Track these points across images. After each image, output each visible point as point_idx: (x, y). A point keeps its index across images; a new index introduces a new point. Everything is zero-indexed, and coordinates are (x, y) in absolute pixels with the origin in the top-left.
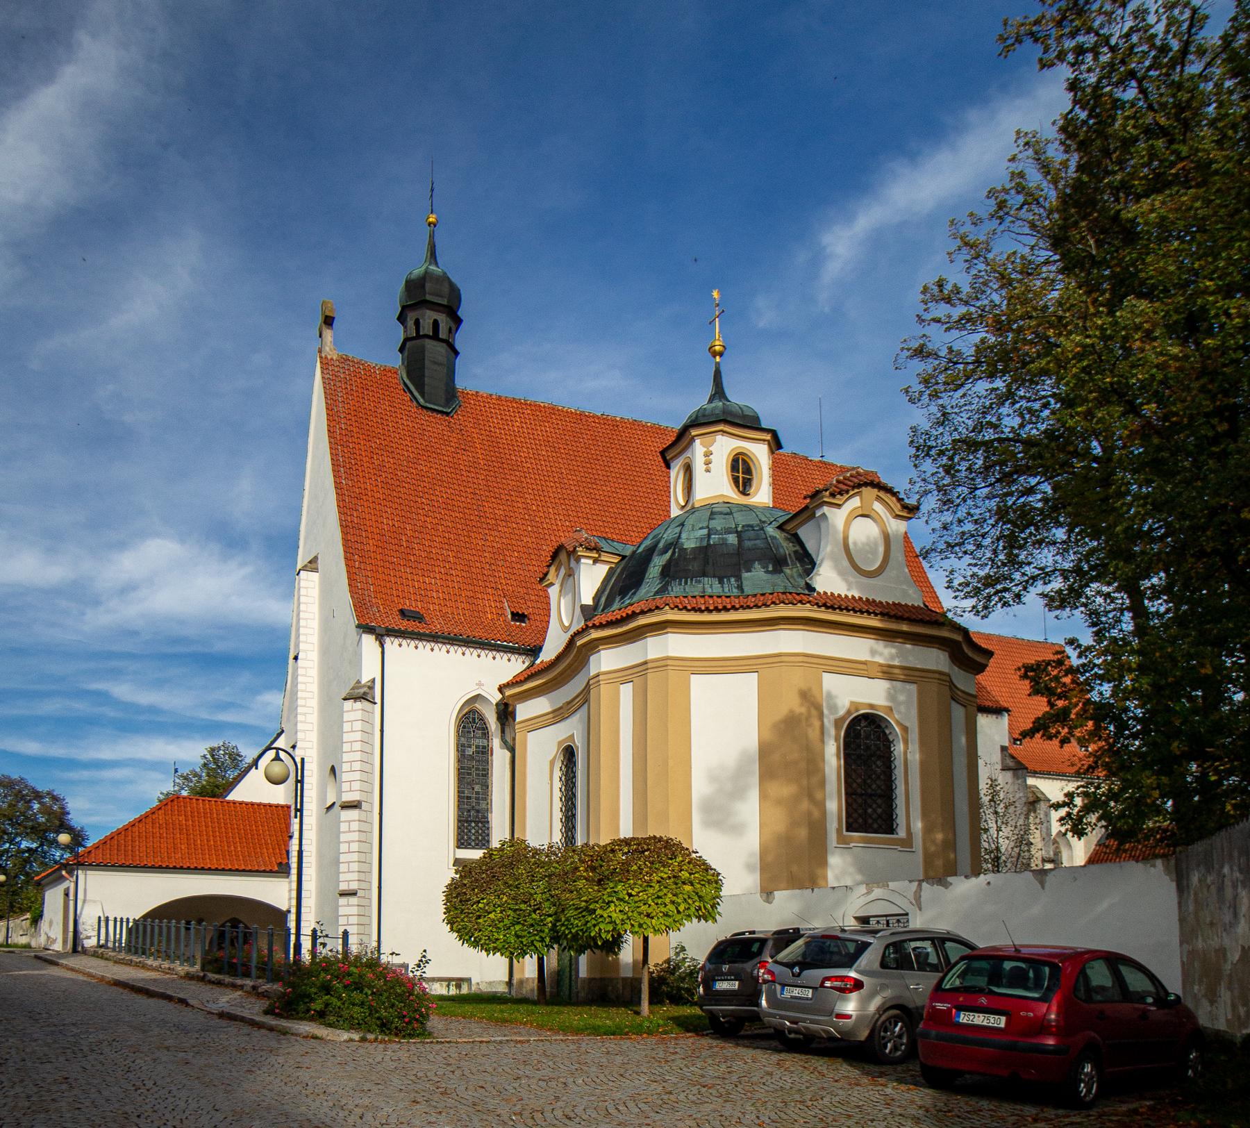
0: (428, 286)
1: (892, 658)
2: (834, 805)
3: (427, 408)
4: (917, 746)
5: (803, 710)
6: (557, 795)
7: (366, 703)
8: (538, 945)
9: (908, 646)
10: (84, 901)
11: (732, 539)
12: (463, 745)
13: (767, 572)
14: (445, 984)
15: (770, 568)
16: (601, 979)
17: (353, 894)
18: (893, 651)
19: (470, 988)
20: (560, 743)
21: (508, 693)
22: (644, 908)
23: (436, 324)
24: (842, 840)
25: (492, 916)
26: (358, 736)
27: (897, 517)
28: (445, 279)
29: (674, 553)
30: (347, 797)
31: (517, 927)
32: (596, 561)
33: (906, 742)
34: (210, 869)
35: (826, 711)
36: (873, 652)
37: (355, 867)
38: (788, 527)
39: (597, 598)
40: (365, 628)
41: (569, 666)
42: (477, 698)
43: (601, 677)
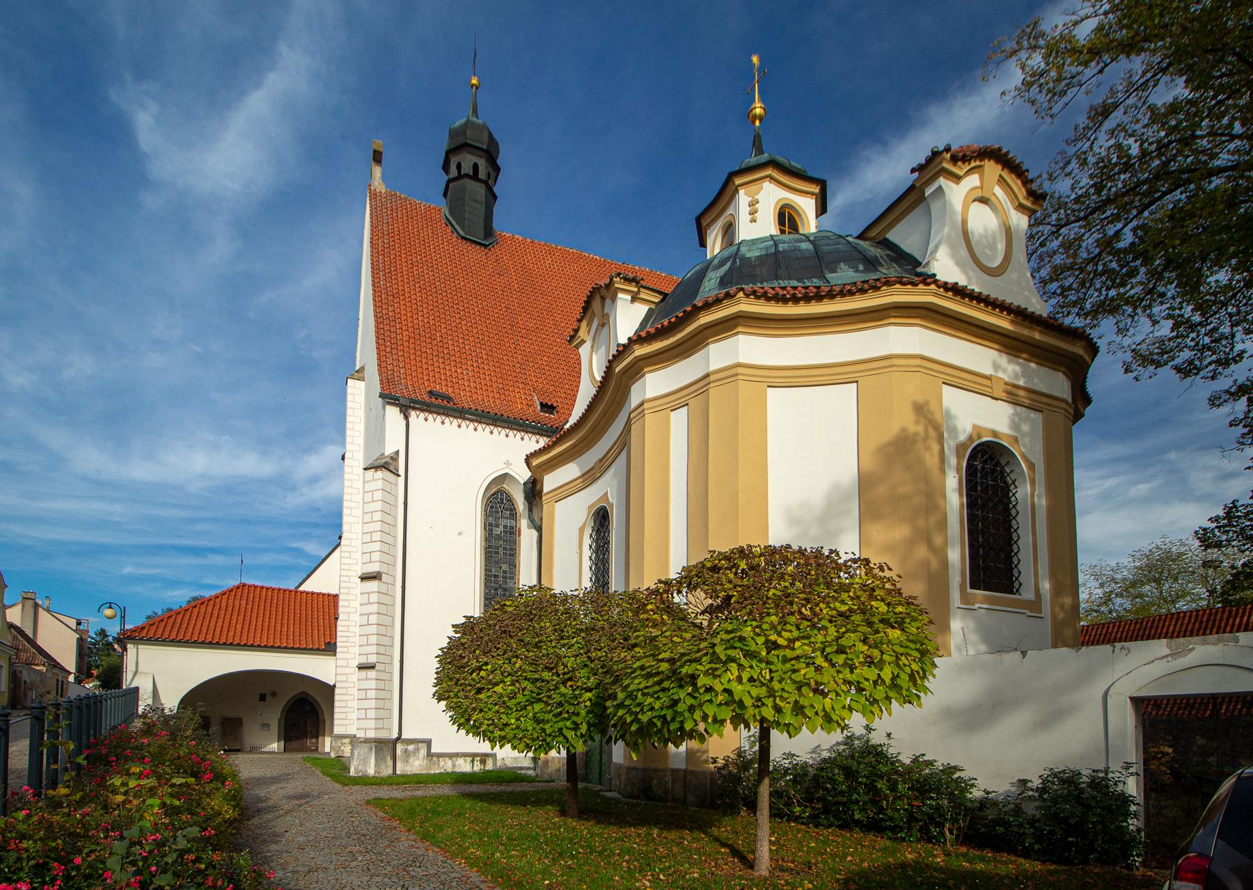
1: (1016, 376)
2: (956, 555)
3: (466, 239)
4: (1043, 490)
5: (920, 429)
6: (587, 563)
7: (388, 473)
8: (570, 734)
9: (1033, 365)
10: (136, 673)
12: (491, 525)
13: (857, 271)
14: (469, 759)
15: (861, 267)
16: (645, 770)
17: (372, 667)
18: (1018, 369)
21: (535, 462)
22: (805, 672)
23: (476, 167)
24: (965, 598)
25: (499, 689)
27: (1021, 207)
28: (484, 127)
29: (734, 262)
31: (538, 707)
32: (634, 300)
33: (1033, 483)
35: (945, 435)
36: (996, 367)
38: (873, 234)
40: (388, 397)
41: (604, 414)
42: (504, 477)
43: (646, 406)
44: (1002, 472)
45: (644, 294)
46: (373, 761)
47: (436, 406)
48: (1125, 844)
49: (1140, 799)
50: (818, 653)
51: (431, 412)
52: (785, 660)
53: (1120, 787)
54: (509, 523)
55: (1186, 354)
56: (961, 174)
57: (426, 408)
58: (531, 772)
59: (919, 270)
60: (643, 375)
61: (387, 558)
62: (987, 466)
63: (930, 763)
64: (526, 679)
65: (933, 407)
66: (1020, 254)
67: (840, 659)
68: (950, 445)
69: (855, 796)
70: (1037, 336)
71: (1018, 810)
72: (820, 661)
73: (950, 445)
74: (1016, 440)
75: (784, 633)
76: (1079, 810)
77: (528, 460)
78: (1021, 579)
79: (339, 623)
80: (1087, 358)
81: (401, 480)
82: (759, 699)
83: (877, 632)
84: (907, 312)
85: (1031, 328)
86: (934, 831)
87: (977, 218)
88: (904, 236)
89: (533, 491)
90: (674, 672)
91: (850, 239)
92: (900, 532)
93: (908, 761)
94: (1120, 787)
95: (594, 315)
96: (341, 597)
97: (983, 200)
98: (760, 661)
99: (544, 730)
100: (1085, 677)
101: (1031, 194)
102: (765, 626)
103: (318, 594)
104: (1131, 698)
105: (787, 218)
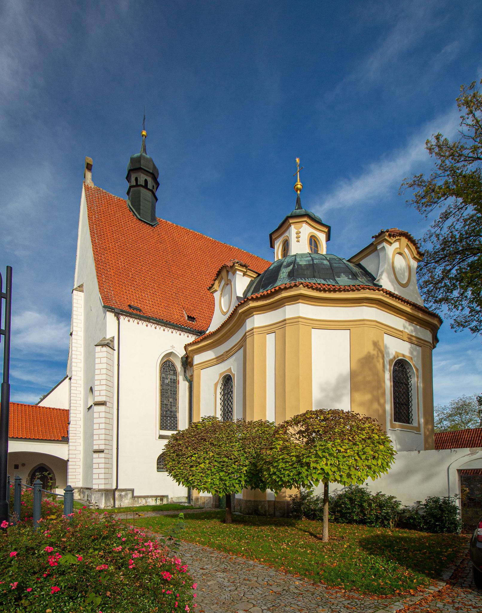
0: (142, 162)
1: (412, 331)
2: (389, 407)
5: (375, 353)
6: (219, 401)
9: (418, 327)
11: (326, 262)
12: (163, 378)
13: (349, 278)
14: (154, 499)
15: (350, 277)
16: (254, 501)
17: (102, 451)
18: (412, 328)
19: (167, 500)
20: (221, 374)
21: (190, 349)
22: (351, 461)
23: (146, 181)
24: (392, 426)
25: (202, 466)
26: (105, 366)
27: (414, 258)
28: (151, 160)
29: (294, 266)
30: (98, 399)
31: (222, 474)
33: (418, 377)
34: (21, 438)
36: (404, 327)
37: (103, 437)
38: (354, 260)
39: (246, 293)
40: (108, 308)
41: (229, 330)
42: (171, 354)
43: (254, 330)
44: (406, 371)
45: (250, 273)
46: (103, 501)
47: (134, 315)
48: (455, 524)
49: (460, 508)
50: (356, 454)
51: (132, 317)
52: (344, 457)
53: (454, 503)
54: (173, 377)
55: (474, 323)
56: (392, 242)
57: (130, 315)
58: (186, 504)
59: (375, 282)
60: (253, 315)
61: (109, 394)
62: (401, 367)
63: (383, 495)
64: (216, 461)
65: (380, 343)
66: (414, 277)
67: (364, 457)
68: (387, 360)
69: (354, 510)
70: (420, 315)
71: (417, 513)
72: (357, 458)
73: (387, 360)
74: (412, 359)
75: (343, 447)
76: (440, 512)
77: (186, 347)
78: (413, 417)
79: (70, 426)
80: (438, 325)
81: (116, 352)
82: (334, 472)
83: (376, 447)
84: (369, 301)
85: (418, 312)
86: (386, 523)
87: (396, 261)
88: (368, 264)
89: (187, 362)
90: (299, 461)
91: (344, 261)
92: (368, 397)
93: (374, 495)
94: (454, 503)
95: (222, 278)
96: (71, 412)
97: (400, 254)
98: (334, 457)
99: (225, 484)
100: (442, 461)
101: (419, 253)
102: (336, 444)
103: (53, 409)
104: (457, 470)
105: (313, 241)
